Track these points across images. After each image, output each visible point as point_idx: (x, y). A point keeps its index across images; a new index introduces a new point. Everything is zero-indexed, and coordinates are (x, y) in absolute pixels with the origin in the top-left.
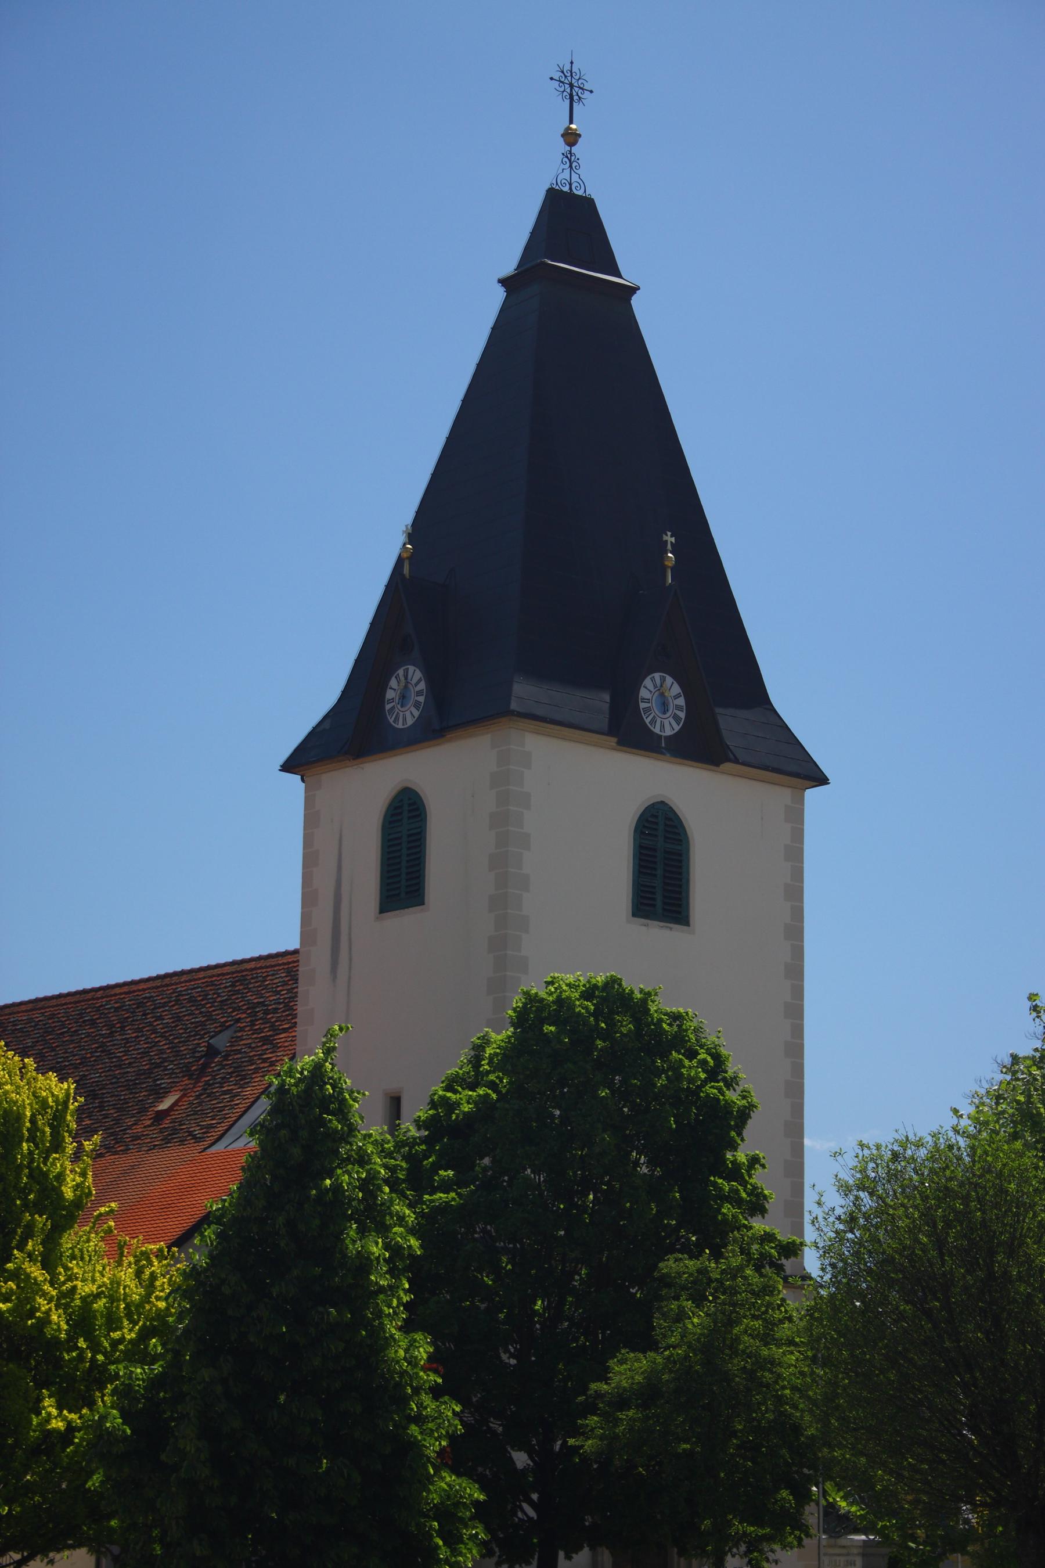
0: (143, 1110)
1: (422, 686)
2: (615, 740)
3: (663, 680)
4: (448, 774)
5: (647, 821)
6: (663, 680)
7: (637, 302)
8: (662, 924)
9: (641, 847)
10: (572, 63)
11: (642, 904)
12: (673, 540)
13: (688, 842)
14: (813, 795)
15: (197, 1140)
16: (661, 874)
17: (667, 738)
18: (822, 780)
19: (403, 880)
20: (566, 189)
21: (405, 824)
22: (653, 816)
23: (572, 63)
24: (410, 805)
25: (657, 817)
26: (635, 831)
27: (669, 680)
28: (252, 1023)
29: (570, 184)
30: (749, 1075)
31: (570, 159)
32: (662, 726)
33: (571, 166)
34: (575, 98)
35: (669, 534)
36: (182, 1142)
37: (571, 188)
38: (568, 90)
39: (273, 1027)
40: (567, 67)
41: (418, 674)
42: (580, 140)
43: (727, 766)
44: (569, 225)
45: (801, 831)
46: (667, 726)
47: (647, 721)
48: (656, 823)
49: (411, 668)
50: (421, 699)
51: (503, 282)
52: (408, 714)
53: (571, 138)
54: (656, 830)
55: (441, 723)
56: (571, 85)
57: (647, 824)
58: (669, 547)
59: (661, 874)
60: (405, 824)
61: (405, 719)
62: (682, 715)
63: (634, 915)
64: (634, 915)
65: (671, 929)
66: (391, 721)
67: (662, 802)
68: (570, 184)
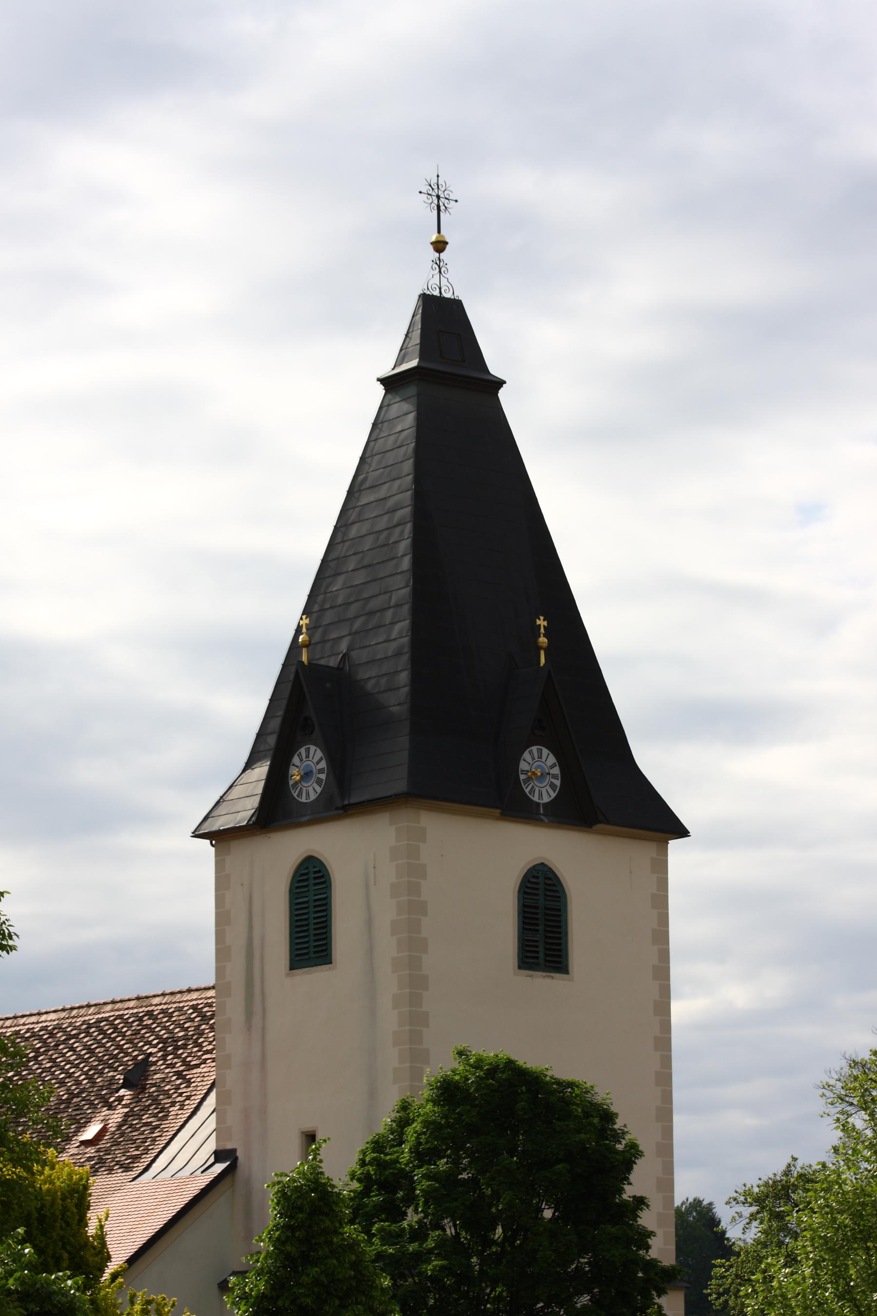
0: (68, 1139)
1: (323, 765)
2: (499, 811)
3: (540, 752)
4: (357, 852)
5: (529, 882)
6: (540, 752)
7: (503, 395)
8: (544, 974)
9: (524, 906)
10: (438, 176)
11: (527, 957)
12: (545, 623)
13: (566, 898)
14: (675, 846)
15: (127, 1168)
16: (543, 930)
17: (545, 805)
18: (682, 832)
19: (311, 941)
20: (436, 293)
21: (311, 886)
22: (534, 877)
23: (438, 176)
24: (315, 872)
25: (537, 877)
26: (519, 892)
27: (545, 751)
28: (164, 1057)
29: (440, 288)
30: (632, 1122)
31: (439, 265)
32: (541, 795)
33: (440, 272)
34: (442, 208)
35: (542, 618)
36: (110, 1170)
37: (440, 292)
38: (436, 202)
39: (184, 1062)
40: (434, 181)
41: (319, 754)
42: (448, 247)
43: (599, 826)
44: (443, 326)
45: (666, 880)
46: (544, 793)
47: (527, 791)
48: (537, 883)
49: (313, 748)
50: (323, 776)
51: (383, 381)
52: (311, 789)
53: (440, 246)
54: (537, 889)
55: (342, 802)
56: (438, 197)
57: (529, 885)
58: (542, 630)
59: (543, 930)
60: (311, 886)
61: (308, 794)
62: (558, 783)
63: (520, 967)
64: (520, 967)
65: (553, 978)
66: (295, 795)
67: (542, 864)
68: (440, 288)
